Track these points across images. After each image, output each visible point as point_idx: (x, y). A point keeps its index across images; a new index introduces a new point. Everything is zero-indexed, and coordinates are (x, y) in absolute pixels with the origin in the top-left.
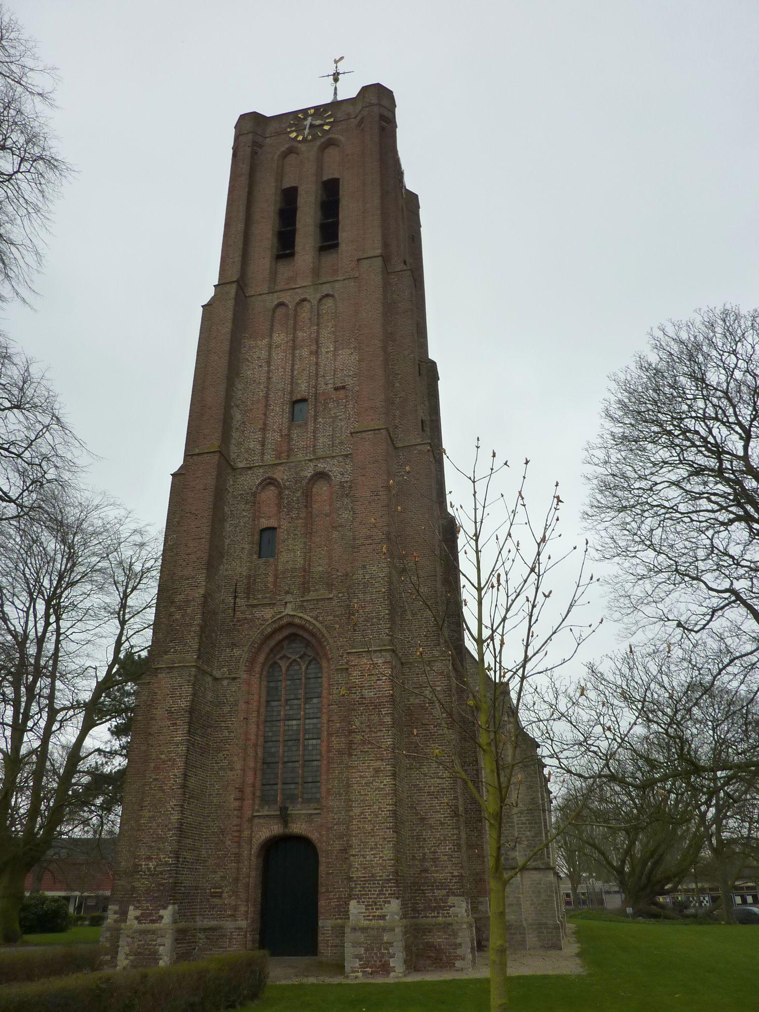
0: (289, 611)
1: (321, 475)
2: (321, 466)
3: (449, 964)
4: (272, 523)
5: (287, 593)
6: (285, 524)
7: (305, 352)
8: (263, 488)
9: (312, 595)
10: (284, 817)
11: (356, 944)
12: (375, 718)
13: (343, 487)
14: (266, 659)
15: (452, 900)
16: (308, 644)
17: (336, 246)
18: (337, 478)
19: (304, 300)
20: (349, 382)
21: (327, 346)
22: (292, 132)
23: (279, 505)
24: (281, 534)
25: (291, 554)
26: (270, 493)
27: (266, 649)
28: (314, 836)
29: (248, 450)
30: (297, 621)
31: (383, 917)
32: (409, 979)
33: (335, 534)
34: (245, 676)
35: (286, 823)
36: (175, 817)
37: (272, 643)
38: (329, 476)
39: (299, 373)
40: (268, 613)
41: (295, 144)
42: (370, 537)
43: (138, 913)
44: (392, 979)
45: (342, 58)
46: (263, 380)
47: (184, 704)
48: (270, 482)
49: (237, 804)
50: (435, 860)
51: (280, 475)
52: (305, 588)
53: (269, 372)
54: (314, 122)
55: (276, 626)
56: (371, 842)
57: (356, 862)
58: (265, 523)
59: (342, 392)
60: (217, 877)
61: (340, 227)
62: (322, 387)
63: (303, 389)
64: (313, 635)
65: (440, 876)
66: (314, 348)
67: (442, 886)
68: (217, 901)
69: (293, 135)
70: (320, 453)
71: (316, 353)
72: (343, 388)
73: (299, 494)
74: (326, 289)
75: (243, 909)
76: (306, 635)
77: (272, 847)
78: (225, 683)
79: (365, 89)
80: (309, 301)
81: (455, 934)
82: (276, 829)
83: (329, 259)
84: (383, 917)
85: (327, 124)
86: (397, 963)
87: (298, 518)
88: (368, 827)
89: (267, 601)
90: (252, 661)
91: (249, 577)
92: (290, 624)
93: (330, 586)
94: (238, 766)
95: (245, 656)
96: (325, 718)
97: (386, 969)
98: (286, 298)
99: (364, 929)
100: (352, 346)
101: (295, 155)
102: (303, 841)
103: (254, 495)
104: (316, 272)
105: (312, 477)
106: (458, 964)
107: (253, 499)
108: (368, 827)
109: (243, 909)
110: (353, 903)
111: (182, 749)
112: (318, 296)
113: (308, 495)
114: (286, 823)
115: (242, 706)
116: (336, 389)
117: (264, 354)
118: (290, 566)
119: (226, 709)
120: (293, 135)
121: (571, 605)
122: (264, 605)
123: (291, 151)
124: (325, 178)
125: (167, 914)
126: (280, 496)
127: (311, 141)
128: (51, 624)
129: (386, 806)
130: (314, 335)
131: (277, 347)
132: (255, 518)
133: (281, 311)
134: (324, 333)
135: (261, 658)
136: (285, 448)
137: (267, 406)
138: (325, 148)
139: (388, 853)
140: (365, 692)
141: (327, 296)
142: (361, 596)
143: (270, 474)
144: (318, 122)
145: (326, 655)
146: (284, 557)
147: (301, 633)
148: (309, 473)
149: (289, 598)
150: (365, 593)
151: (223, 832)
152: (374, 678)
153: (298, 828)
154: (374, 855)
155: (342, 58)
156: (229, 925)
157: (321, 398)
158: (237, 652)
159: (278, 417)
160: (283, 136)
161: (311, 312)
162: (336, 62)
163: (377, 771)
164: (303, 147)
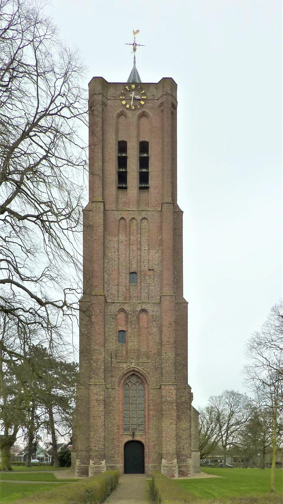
0: (133, 365)
1: (144, 311)
2: (144, 306)
3: (186, 475)
4: (124, 329)
5: (132, 358)
6: (130, 331)
7: (134, 248)
8: (119, 313)
9: (141, 360)
10: (133, 435)
11: (164, 470)
12: (171, 407)
13: (153, 317)
14: (124, 382)
15: (188, 459)
16: (139, 378)
17: (147, 188)
18: (151, 313)
19: (133, 218)
20: (155, 267)
21: (145, 247)
22: (123, 100)
23: (127, 322)
24: (128, 334)
25: (132, 343)
26: (122, 315)
27: (124, 379)
28: (143, 441)
29: (112, 294)
30: (136, 369)
31: (172, 463)
32: (180, 479)
33: (150, 337)
34: (117, 388)
35: (133, 437)
36: (103, 435)
37: (126, 376)
38: (147, 311)
39: (132, 258)
40: (125, 365)
41: (125, 110)
42: (168, 342)
43: (93, 462)
44: (175, 478)
45: (138, 31)
46: (116, 259)
48: (122, 310)
49: (118, 430)
50: (183, 449)
51: (126, 308)
52: (138, 358)
53: (119, 255)
54: (136, 96)
55: (128, 371)
56: (169, 443)
57: (164, 449)
58: (120, 328)
59: (152, 272)
60: (113, 452)
61: (150, 176)
62: (143, 268)
63: (134, 268)
64: (142, 375)
65: (185, 453)
66: (139, 246)
67: (185, 456)
68: (113, 459)
69: (124, 102)
70: (143, 300)
71: (140, 249)
72: (152, 270)
73: (135, 318)
74: (144, 215)
75: (121, 461)
76: (139, 375)
77: (127, 444)
78: (110, 390)
79: (164, 79)
80: (136, 220)
81: (188, 468)
82: (130, 438)
83: (144, 194)
84: (172, 463)
85: (143, 100)
86: (176, 475)
87: (135, 328)
88: (168, 439)
89: (123, 361)
91: (116, 350)
92: (134, 371)
93: (148, 357)
94: (117, 419)
95: (117, 381)
96: (147, 405)
97: (173, 476)
98: (125, 215)
99: (167, 467)
100: (156, 249)
101: (124, 117)
102: (140, 443)
103: (116, 315)
104: (138, 202)
105: (140, 311)
106: (189, 475)
107: (115, 317)
108: (168, 439)
109: (121, 461)
110: (163, 460)
111: (103, 413)
112: (141, 218)
113: (138, 318)
114: (133, 437)
115: (117, 399)
116: (149, 270)
117: (116, 246)
118: (133, 348)
119: (111, 399)
120: (124, 102)
121: (222, 369)
122: (123, 362)
123: (122, 114)
124: (141, 140)
125: (103, 462)
126: (127, 317)
127: (133, 110)
128: (11, 356)
129: (174, 433)
130: (139, 240)
131: (121, 242)
132: (117, 326)
133: (122, 222)
134: (144, 239)
135: (122, 382)
136: (128, 296)
137: (119, 273)
138: (141, 117)
139: (174, 446)
140: (167, 398)
141: (145, 218)
142: (165, 364)
143: (122, 307)
144: (138, 97)
145: (147, 382)
146: (130, 344)
147: (137, 374)
148: (139, 309)
149: (133, 361)
150: (166, 363)
151: (113, 439)
153: (138, 438)
154: (169, 446)
155: (138, 31)
156: (118, 465)
157: (143, 273)
158: (114, 379)
159: (124, 279)
160: (118, 101)
161: (137, 226)
162: (135, 33)
163: (171, 423)
164: (129, 113)
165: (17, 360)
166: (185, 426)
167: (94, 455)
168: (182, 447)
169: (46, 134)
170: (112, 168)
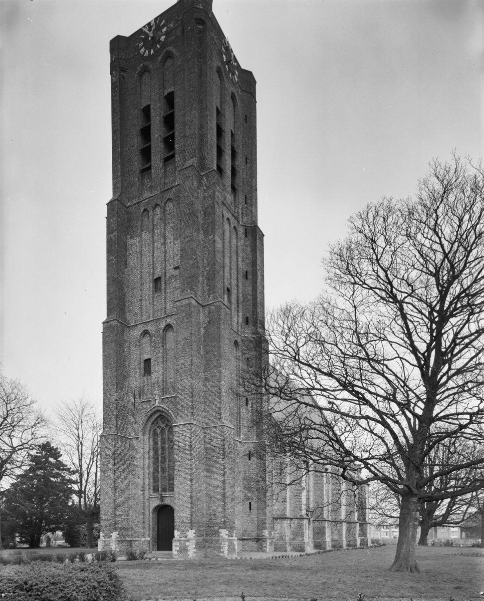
0: (157, 404)
15: (220, 530)
27: (150, 423)
30: (160, 409)
37: (153, 419)
47: (111, 451)
48: (146, 333)
49: (142, 492)
58: (146, 357)
67: (217, 525)
90: (144, 429)
92: (158, 411)
105: (165, 327)
148: (163, 325)
152: (184, 437)
159: (149, 286)
163: (185, 479)
165: (472, 494)
166: (216, 481)
167: (104, 525)
168: (213, 513)
169: (468, 417)
170: (136, 142)
